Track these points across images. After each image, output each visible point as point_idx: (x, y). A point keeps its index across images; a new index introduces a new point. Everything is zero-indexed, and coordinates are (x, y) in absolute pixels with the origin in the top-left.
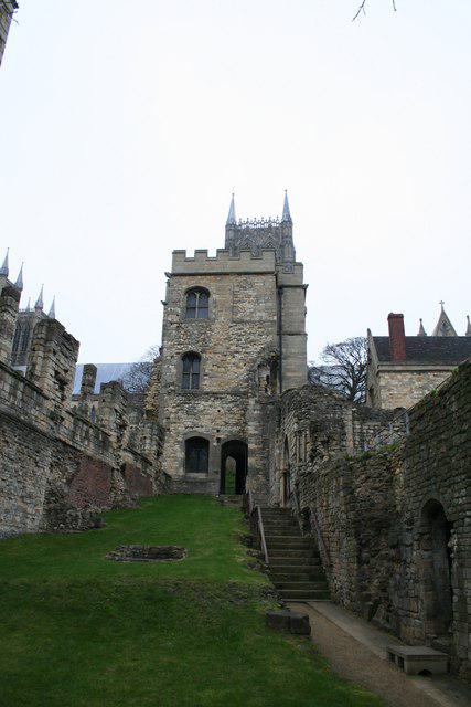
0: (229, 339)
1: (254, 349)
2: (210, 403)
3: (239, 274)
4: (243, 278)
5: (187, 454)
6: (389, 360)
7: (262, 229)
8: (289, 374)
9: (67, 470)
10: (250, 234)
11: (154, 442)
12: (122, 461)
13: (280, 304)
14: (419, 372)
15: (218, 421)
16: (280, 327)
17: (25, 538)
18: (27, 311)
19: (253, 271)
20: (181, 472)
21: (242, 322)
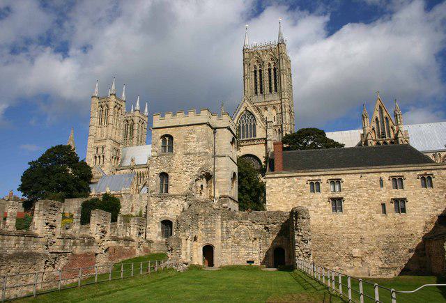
3: (188, 125)
4: (190, 127)
12: (106, 247)
21: (189, 154)
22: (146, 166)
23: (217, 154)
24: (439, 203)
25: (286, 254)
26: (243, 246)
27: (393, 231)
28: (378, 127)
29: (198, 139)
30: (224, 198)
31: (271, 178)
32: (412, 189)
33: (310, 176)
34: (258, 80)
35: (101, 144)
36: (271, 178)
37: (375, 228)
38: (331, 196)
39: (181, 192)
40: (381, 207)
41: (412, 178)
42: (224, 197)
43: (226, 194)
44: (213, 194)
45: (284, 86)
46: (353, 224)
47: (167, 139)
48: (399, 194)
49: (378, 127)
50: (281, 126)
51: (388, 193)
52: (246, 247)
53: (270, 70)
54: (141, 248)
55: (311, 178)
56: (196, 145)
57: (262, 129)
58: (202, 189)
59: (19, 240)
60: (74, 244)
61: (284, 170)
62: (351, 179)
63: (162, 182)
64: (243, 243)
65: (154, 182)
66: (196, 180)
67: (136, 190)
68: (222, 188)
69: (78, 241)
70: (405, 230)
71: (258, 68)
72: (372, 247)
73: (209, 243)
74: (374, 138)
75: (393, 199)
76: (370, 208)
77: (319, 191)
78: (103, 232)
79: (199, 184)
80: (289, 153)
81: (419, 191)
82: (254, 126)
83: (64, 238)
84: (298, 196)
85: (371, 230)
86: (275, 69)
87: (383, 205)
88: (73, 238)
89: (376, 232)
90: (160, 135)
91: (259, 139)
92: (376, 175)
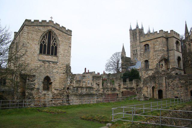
0: (154, 56)
3: (155, 39)
4: (155, 40)
8: (171, 61)
16: (168, 49)
17: (134, 79)
21: (156, 51)
29: (159, 44)
35: (135, 49)
42: (174, 68)
44: (168, 67)
56: (158, 47)
59: (87, 89)
60: (108, 90)
63: (146, 64)
64: (176, 89)
68: (172, 64)
69: (109, 89)
73: (160, 89)
78: (119, 85)
83: (104, 89)
88: (107, 88)
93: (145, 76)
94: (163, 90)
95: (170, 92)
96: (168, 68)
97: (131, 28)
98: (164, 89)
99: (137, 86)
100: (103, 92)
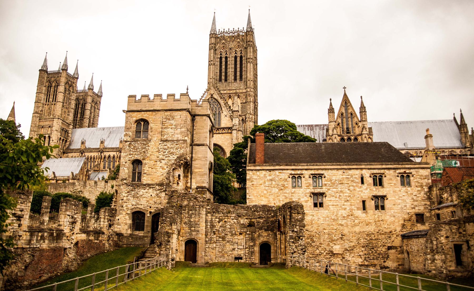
0: (159, 151)
1: (173, 158)
2: (146, 190)
3: (166, 110)
4: (168, 113)
5: (133, 220)
6: (254, 162)
7: (233, 36)
9: (25, 261)
10: (225, 40)
11: (106, 220)
12: (74, 242)
13: (193, 126)
14: (270, 170)
15: (151, 202)
16: (192, 141)
18: (84, 91)
19: (174, 108)
20: (129, 232)
21: (166, 141)
22: (119, 150)
23: (195, 142)
24: (417, 201)
25: (272, 251)
26: (228, 242)
27: (372, 228)
28: (342, 123)
30: (201, 190)
31: (252, 170)
32: (392, 187)
33: (293, 170)
34: (223, 67)
36: (252, 170)
37: (355, 225)
38: (313, 191)
39: (157, 181)
40: (361, 204)
41: (391, 177)
42: (202, 188)
43: (204, 185)
44: (189, 185)
45: (250, 75)
46: (334, 220)
47: (142, 123)
48: (380, 191)
49: (342, 123)
50: (245, 115)
51: (368, 191)
52: (232, 243)
53: (236, 58)
54: (110, 242)
55: (293, 172)
57: (228, 118)
58: (179, 179)
61: (265, 162)
62: (333, 175)
63: (134, 170)
64: (229, 237)
65: (125, 172)
66: (174, 169)
67: (86, 176)
68: (199, 178)
69: (46, 234)
70: (385, 227)
71: (224, 55)
72: (352, 244)
74: (339, 134)
75: (374, 196)
76: (351, 205)
77: (409, 184)
79: (177, 174)
80: (285, 144)
81: (399, 189)
82: (219, 114)
83: (32, 231)
84: (279, 191)
85: (352, 227)
86: (241, 57)
87: (364, 202)
88: (42, 231)
89: (357, 229)
90: (135, 119)
91: (224, 128)
92: (358, 172)
93: (128, 200)
94: (200, 241)
95: (214, 245)
96: (187, 187)
97: (45, 65)
98: (201, 238)
99: (110, 226)
100: (29, 242)
